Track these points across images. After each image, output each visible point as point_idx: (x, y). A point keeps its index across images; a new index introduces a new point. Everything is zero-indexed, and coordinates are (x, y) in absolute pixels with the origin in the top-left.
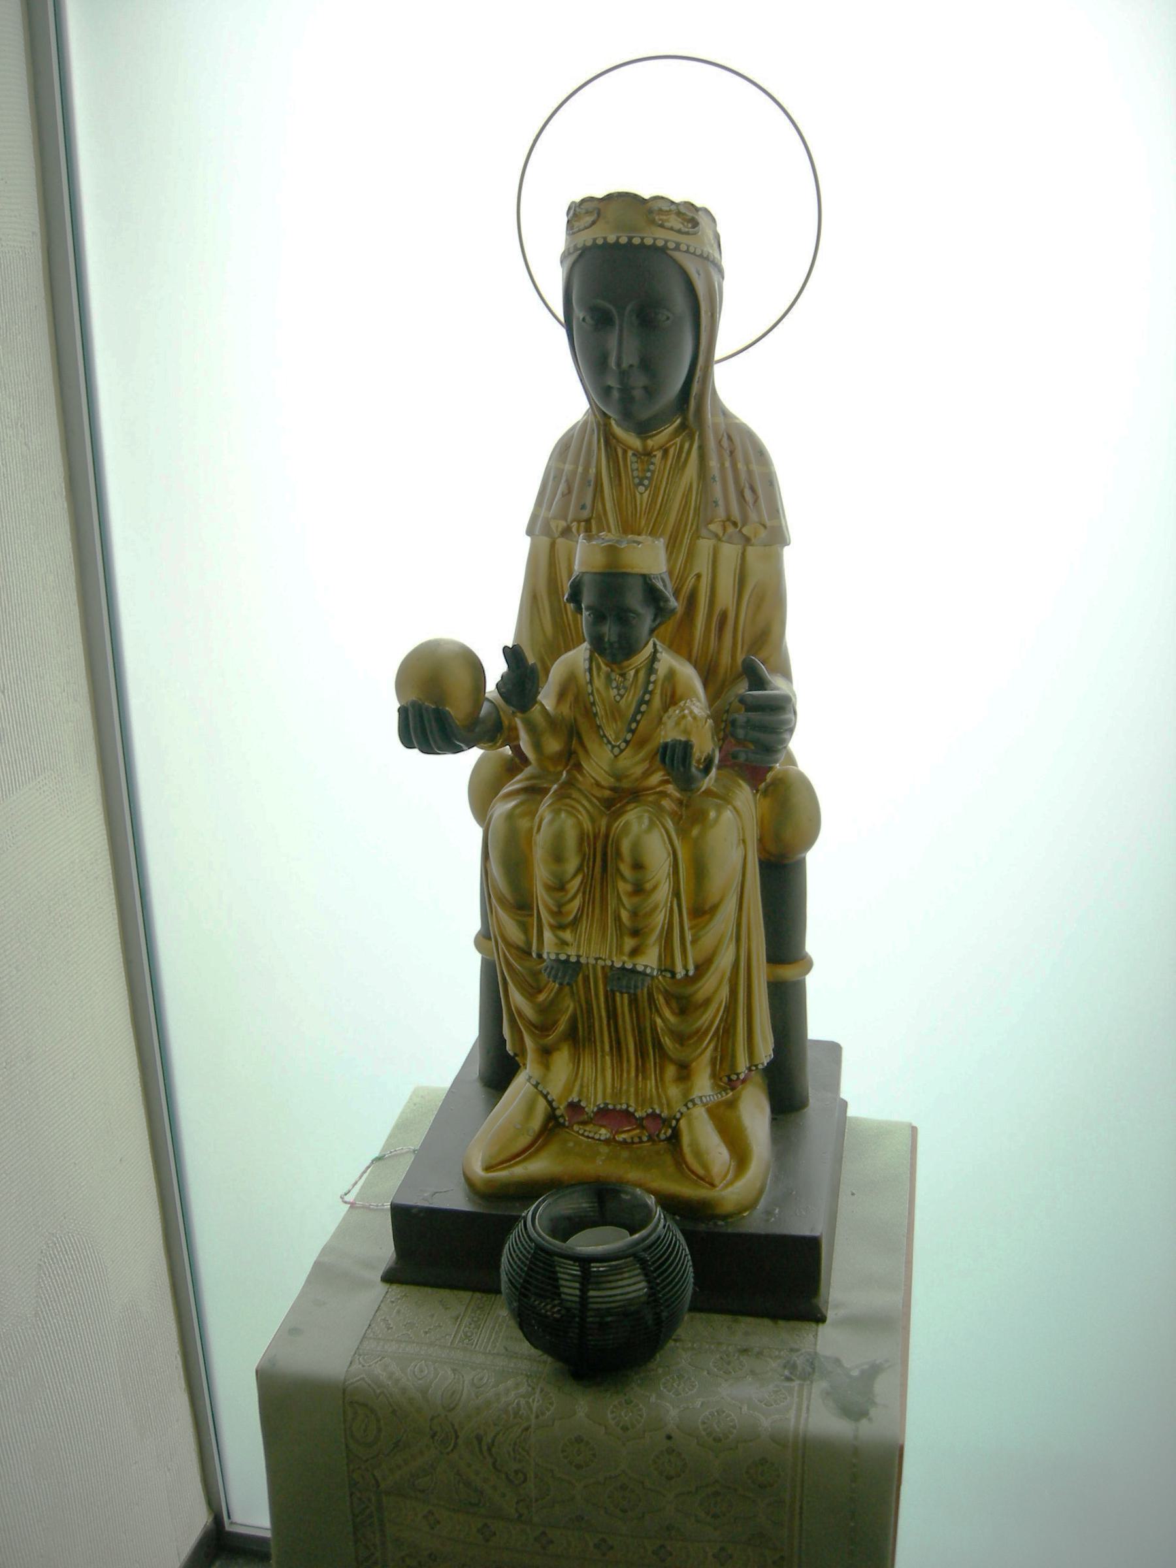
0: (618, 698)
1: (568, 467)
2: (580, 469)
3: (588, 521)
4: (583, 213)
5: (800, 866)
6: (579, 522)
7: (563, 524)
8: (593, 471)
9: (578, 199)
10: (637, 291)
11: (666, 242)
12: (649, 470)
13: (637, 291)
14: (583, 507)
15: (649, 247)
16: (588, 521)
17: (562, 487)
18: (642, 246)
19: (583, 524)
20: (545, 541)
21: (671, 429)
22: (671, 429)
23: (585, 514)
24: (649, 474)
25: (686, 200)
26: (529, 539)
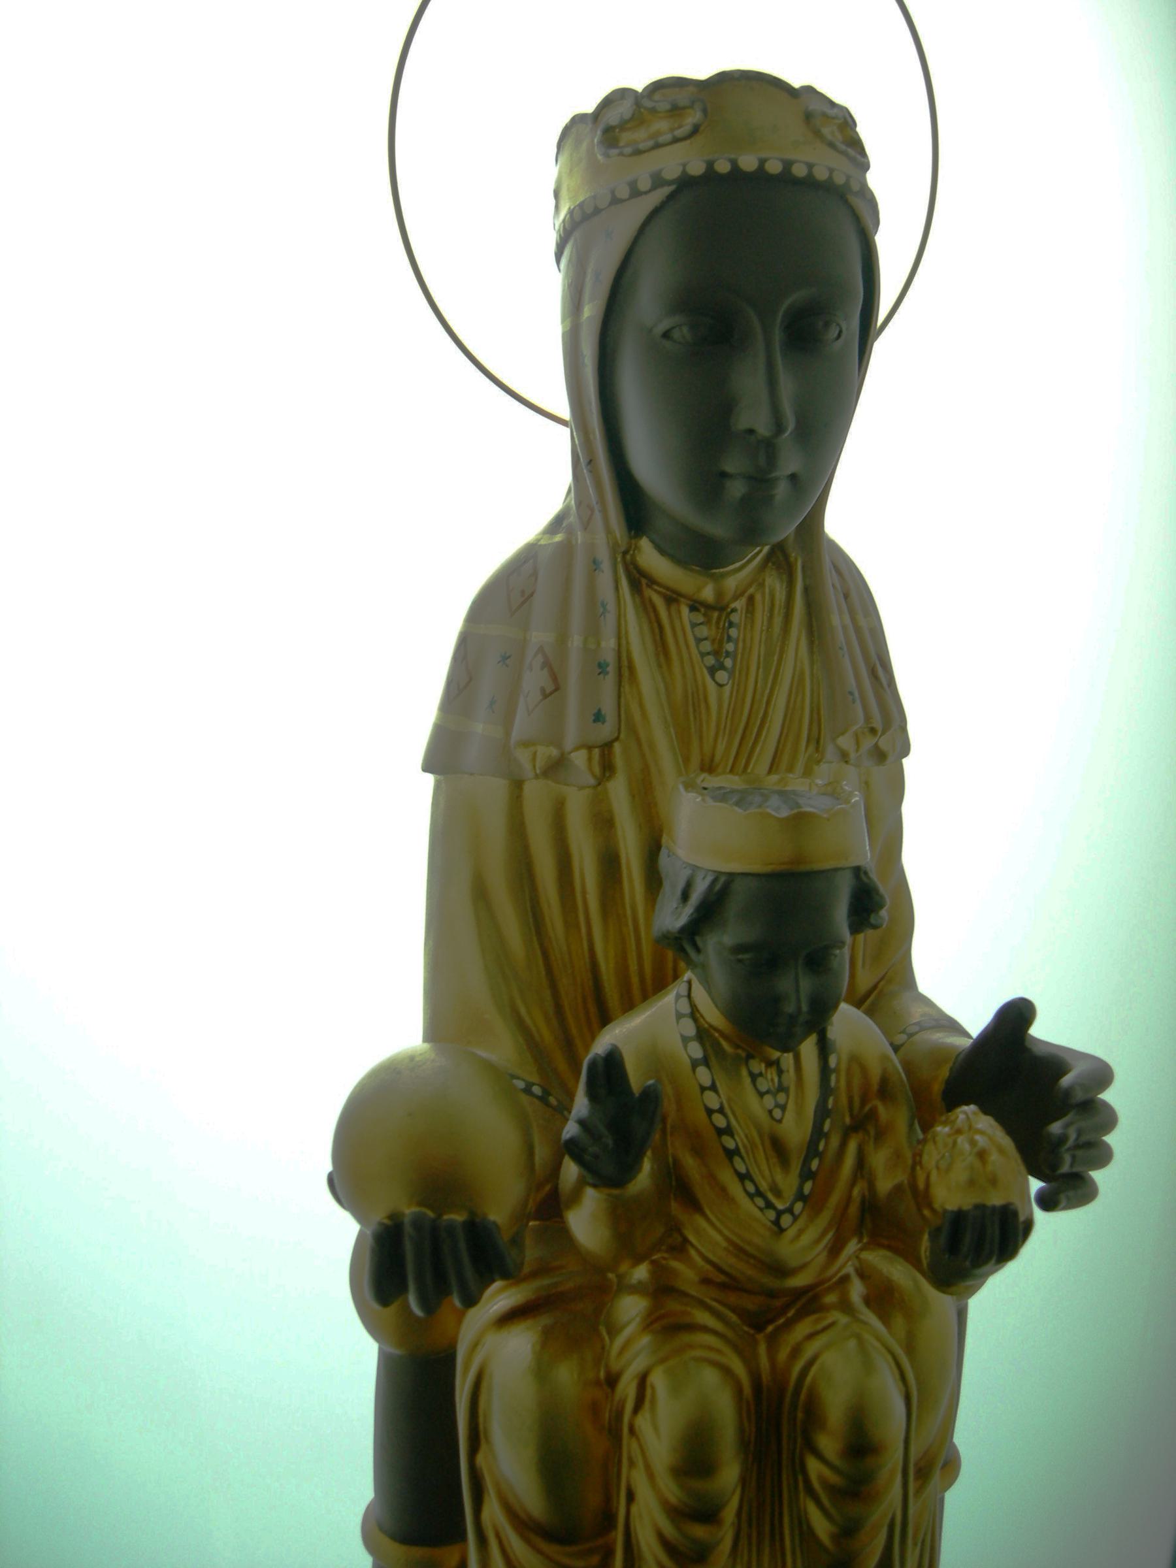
0: (777, 1113)
1: (540, 636)
2: (576, 641)
3: (606, 748)
4: (617, 129)
5: (942, 1500)
6: (590, 748)
7: (545, 753)
8: (609, 643)
9: (862, 130)
10: (730, 271)
11: (810, 166)
12: (729, 639)
13: (730, 271)
14: (598, 717)
15: (722, 178)
16: (606, 748)
17: (534, 680)
18: (760, 176)
19: (596, 752)
20: (496, 790)
21: (618, 536)
22: (618, 536)
23: (606, 731)
24: (730, 647)
25: (700, 57)
26: (429, 779)
